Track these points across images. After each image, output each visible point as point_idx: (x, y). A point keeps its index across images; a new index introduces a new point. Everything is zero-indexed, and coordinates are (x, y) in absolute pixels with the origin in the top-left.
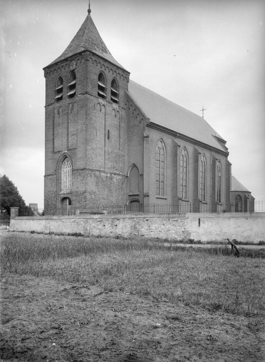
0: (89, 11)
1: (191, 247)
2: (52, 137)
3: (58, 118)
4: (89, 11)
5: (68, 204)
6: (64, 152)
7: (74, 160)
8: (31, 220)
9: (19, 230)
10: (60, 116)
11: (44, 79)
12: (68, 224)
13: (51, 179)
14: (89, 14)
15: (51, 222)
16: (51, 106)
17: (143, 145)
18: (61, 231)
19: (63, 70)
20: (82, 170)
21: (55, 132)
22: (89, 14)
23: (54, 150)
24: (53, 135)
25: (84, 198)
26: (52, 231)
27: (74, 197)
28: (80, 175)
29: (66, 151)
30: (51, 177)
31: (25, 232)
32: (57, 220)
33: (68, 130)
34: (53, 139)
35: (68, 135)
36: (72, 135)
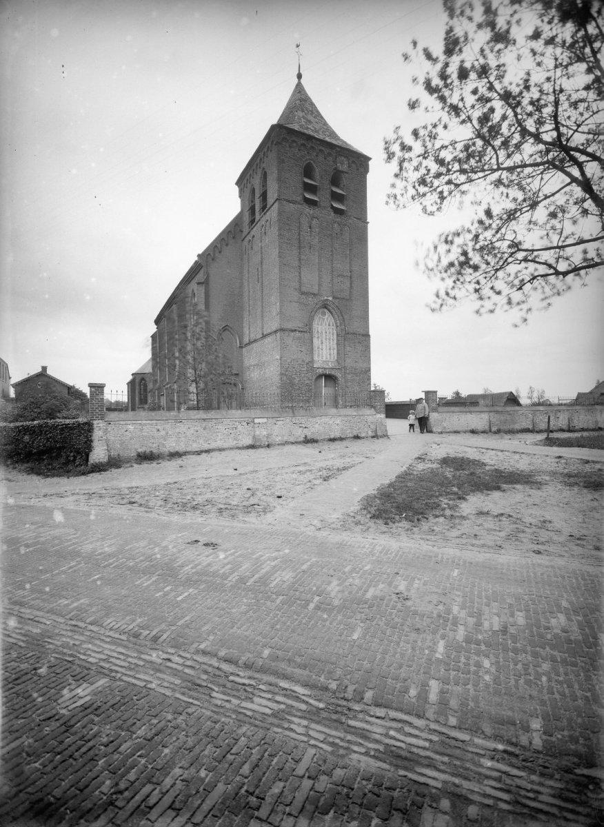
13: (299, 338)
16: (294, 206)
28: (359, 342)
29: (330, 298)
30: (298, 334)
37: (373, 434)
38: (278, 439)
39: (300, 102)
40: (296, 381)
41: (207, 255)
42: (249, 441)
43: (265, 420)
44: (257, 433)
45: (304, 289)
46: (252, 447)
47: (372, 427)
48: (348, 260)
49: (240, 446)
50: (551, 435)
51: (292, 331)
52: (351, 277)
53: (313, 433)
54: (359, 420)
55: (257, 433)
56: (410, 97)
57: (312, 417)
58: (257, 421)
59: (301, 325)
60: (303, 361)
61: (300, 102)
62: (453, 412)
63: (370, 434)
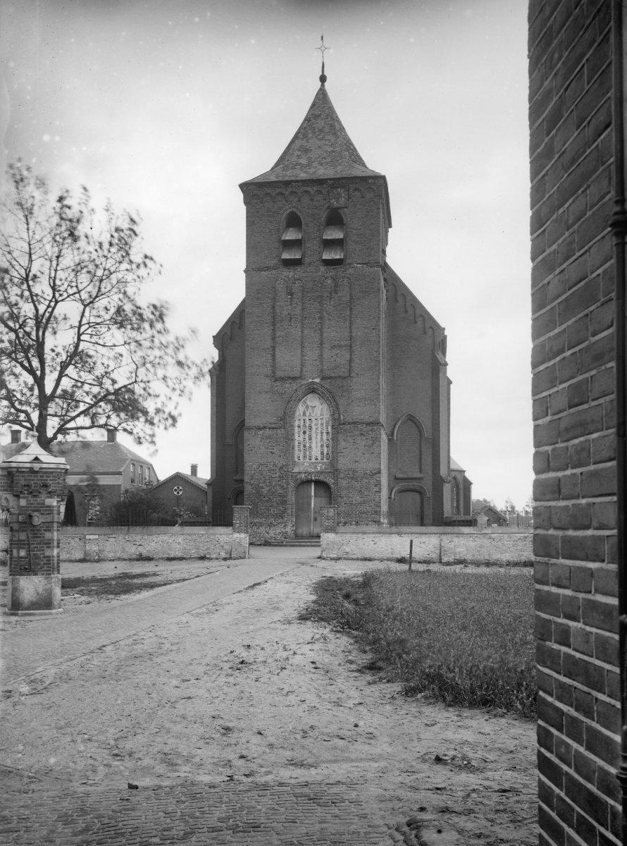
0: (323, 79)
1: (429, 571)
2: (269, 343)
3: (288, 303)
4: (323, 79)
5: (313, 494)
6: (311, 380)
7: (341, 402)
8: (393, 535)
9: (355, 557)
10: (294, 300)
11: (243, 209)
12: (506, 543)
13: (269, 437)
14: (323, 85)
15: (456, 539)
16: (266, 273)
17: (602, 397)
18: (487, 557)
19: (306, 200)
20: (368, 424)
21: (279, 333)
22: (323, 85)
23: (274, 372)
24: (273, 339)
25: (376, 486)
26: (462, 556)
27: (345, 482)
28: (362, 434)
29: (317, 380)
30: (268, 432)
31: (496, 564)
32: (476, 535)
33: (322, 335)
34: (274, 348)
35: (321, 344)
36: (333, 347)
37: (228, 556)
38: (110, 556)
39: (321, 120)
40: (265, 491)
41: (224, 335)
42: (79, 555)
43: (97, 537)
44: (88, 548)
45: (279, 374)
46: (81, 561)
47: (226, 547)
48: (347, 324)
49: (73, 559)
50: (414, 567)
51: (260, 429)
52: (351, 346)
53: (148, 551)
54: (208, 540)
55: (88, 548)
56: (141, 235)
57: (148, 535)
58: (87, 537)
59: (273, 420)
60: (275, 465)
61: (321, 120)
62: (364, 533)
63: (223, 555)
